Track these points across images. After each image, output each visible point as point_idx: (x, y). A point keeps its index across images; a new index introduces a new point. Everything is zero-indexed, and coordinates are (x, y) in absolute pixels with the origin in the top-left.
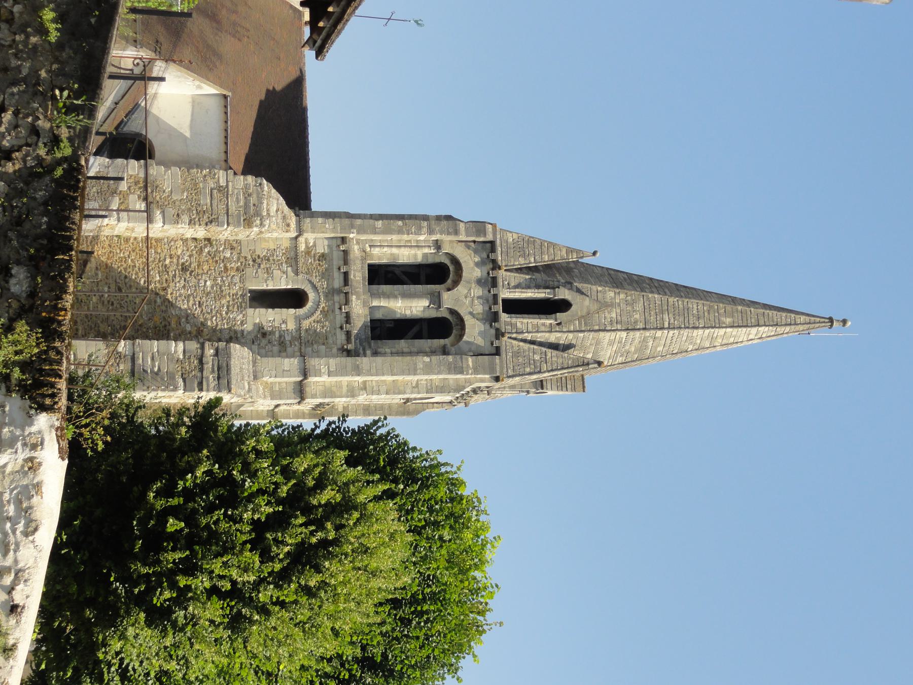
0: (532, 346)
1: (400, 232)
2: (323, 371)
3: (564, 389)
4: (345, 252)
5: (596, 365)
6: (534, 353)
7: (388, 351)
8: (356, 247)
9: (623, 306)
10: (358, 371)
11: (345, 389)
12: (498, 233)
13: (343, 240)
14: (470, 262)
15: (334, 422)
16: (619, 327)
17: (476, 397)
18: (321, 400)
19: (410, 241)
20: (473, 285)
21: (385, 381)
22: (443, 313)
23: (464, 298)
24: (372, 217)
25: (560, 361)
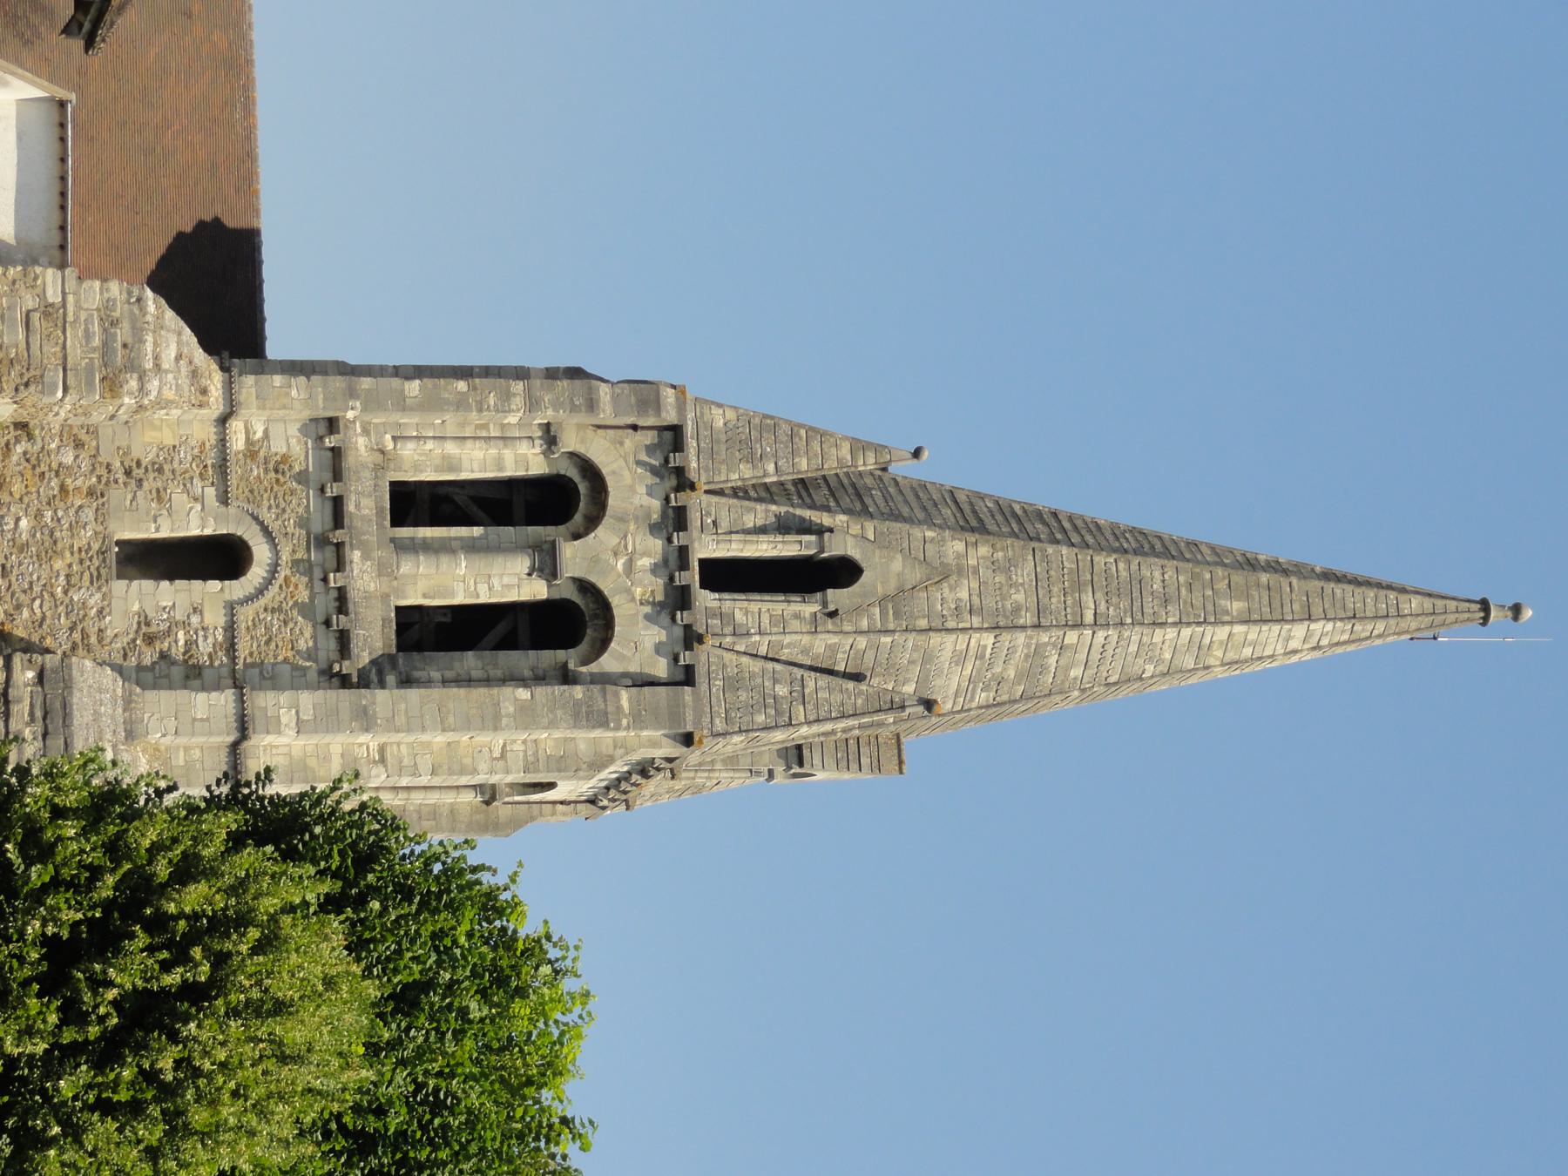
0: (770, 665)
1: (461, 404)
2: (284, 720)
3: (854, 766)
4: (336, 452)
5: (921, 708)
6: (775, 681)
7: (436, 675)
8: (361, 442)
10: (365, 719)
12: (690, 407)
13: (332, 424)
14: (632, 489)
16: (976, 621)
19: (485, 427)
20: (632, 527)
23: (617, 558)
24: (399, 372)
25: (837, 698)
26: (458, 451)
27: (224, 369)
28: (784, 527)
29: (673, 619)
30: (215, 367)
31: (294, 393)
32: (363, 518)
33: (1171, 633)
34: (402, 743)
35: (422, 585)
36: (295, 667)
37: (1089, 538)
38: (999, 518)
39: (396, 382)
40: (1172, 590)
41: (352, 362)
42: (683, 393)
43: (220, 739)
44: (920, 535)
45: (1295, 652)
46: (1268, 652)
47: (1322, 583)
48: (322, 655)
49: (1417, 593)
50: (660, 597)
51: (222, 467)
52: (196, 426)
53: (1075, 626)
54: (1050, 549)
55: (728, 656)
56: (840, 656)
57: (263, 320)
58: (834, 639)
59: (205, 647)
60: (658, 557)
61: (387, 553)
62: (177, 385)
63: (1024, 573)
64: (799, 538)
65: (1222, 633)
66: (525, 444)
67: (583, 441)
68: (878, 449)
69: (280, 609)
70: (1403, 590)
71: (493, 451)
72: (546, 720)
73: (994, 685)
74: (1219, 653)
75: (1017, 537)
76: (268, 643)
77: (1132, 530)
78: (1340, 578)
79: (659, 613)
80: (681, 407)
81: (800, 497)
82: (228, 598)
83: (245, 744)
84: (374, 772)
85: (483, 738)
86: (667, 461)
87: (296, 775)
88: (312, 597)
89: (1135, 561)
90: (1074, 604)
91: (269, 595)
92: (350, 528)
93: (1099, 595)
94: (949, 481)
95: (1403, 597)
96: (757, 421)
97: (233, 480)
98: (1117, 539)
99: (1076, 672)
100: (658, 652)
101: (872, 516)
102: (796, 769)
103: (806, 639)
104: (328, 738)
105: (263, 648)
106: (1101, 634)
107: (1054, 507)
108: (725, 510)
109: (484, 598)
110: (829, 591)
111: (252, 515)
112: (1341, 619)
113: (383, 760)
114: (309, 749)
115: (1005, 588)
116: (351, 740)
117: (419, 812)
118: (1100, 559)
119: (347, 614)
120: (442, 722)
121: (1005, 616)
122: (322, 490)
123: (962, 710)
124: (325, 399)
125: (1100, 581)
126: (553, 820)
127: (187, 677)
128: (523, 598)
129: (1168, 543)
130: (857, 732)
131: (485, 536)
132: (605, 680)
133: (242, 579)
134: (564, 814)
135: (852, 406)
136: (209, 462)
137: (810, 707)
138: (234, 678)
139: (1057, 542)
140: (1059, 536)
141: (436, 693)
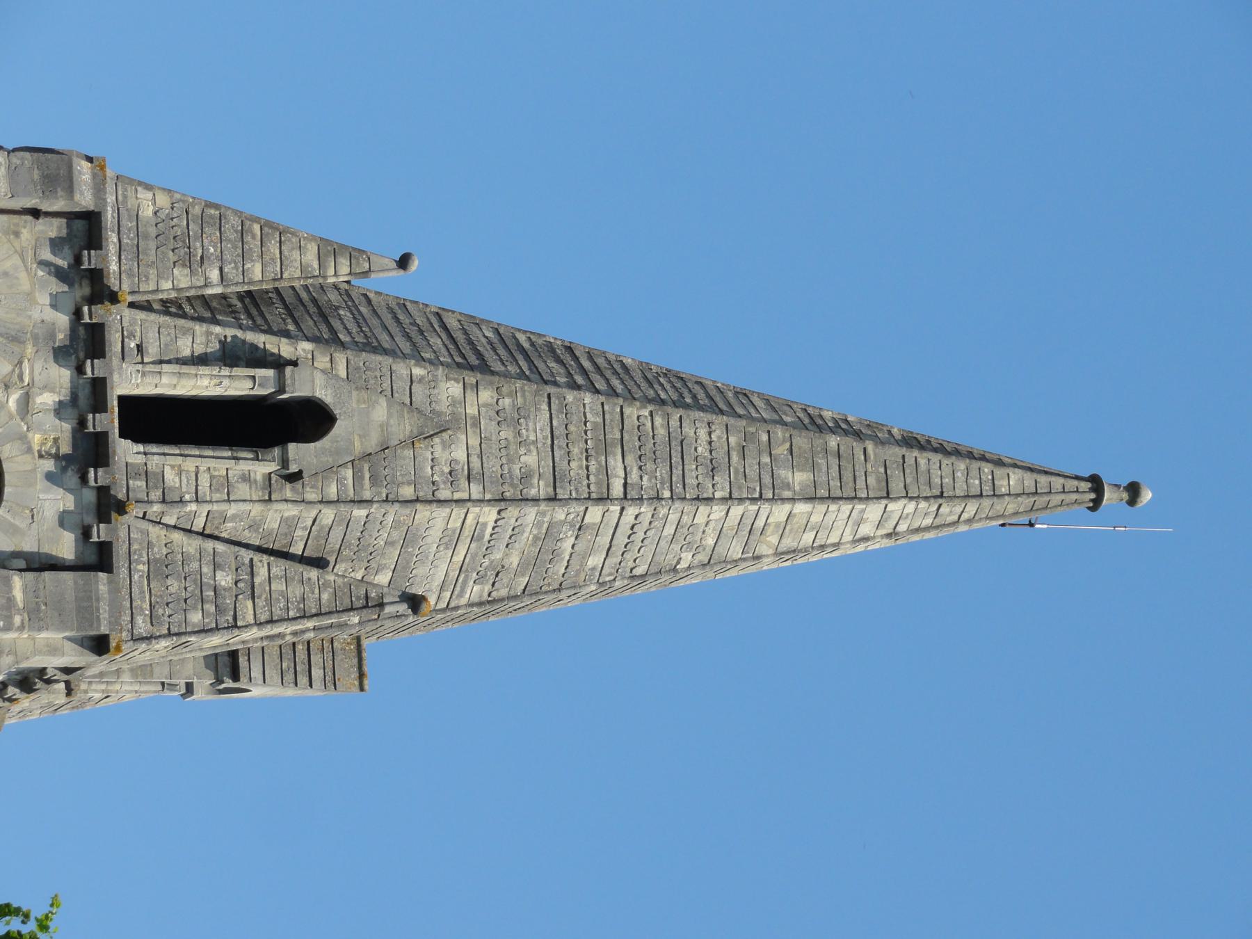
0: (209, 545)
3: (303, 680)
5: (403, 608)
6: (216, 567)
12: (110, 187)
20: (30, 350)
25: (296, 591)
28: (231, 356)
29: (84, 479)
33: (718, 511)
37: (615, 382)
38: (502, 351)
40: (720, 454)
42: (102, 168)
44: (405, 372)
45: (865, 539)
46: (833, 539)
47: (903, 451)
49: (1015, 466)
50: (66, 449)
53: (600, 500)
54: (570, 396)
55: (155, 531)
56: (299, 533)
58: (291, 511)
60: (64, 394)
63: (537, 427)
64: (251, 372)
65: (780, 512)
68: (354, 254)
70: (999, 463)
73: (491, 576)
74: (774, 539)
75: (528, 379)
77: (667, 374)
78: (923, 445)
79: (64, 469)
80: (99, 187)
81: (250, 316)
86: (78, 260)
89: (676, 414)
90: (598, 471)
93: (630, 459)
95: (999, 472)
96: (197, 210)
98: (651, 385)
99: (595, 561)
100: (62, 524)
101: (343, 345)
102: (229, 684)
103: (257, 509)
106: (631, 511)
107: (568, 338)
108: (151, 330)
110: (292, 447)
112: (926, 498)
115: (513, 447)
118: (631, 412)
121: (512, 485)
125: (631, 441)
129: (713, 393)
130: (311, 635)
135: (320, 201)
137: (261, 603)
139: (579, 388)
140: (580, 380)
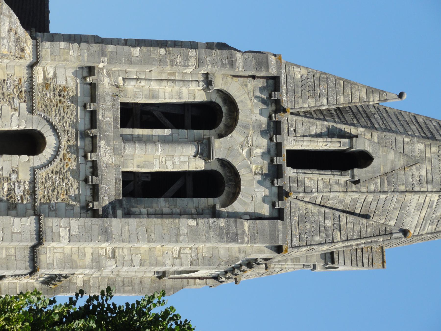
0: (323, 209)
1: (162, 61)
2: (62, 234)
3: (360, 264)
4: (93, 86)
5: (400, 235)
6: (325, 218)
7: (144, 211)
8: (106, 80)
9: (435, 161)
10: (106, 235)
11: (88, 258)
12: (283, 66)
13: (91, 70)
14: (251, 111)
15: (96, 298)
16: (430, 188)
17: (249, 272)
18: (57, 272)
19: (173, 74)
20: (251, 132)
21: (139, 249)
22: (215, 166)
23: (243, 148)
24: (126, 42)
25: (357, 228)
26: (158, 87)
27: (34, 38)
28: (331, 134)
29: (273, 183)
30: (28, 36)
31: (71, 52)
32: (107, 123)
34: (124, 249)
35: (137, 160)
36: (68, 205)
39: (127, 48)
41: (102, 36)
42: (280, 59)
43: (26, 244)
44: (401, 140)
48: (83, 199)
50: (265, 171)
51: (31, 92)
52: (17, 69)
55: (301, 204)
56: (358, 204)
57: (48, 12)
58: (356, 196)
59: (19, 192)
60: (265, 149)
61: (118, 142)
62: (9, 46)
66: (195, 84)
67: (225, 83)
69: (60, 172)
71: (177, 88)
72: (204, 238)
73: (436, 221)
76: (53, 190)
79: (265, 179)
80: (279, 67)
81: (339, 117)
82: (32, 165)
83: (40, 247)
84: (109, 263)
85: (169, 246)
86: (270, 96)
87: (67, 265)
88: (78, 167)
91: (54, 164)
92: (99, 128)
94: (414, 111)
96: (318, 75)
97: (36, 99)
100: (264, 201)
102: (330, 265)
103: (342, 195)
104: (85, 245)
105: (51, 193)
109: (170, 169)
110: (356, 170)
111: (46, 119)
113: (114, 257)
114: (74, 250)
116: (97, 246)
117: (123, 282)
119: (97, 176)
120: (148, 237)
122: (85, 106)
123: (418, 235)
124: (88, 56)
126: (193, 287)
127: (9, 209)
128: (191, 169)
130: (363, 246)
131: (172, 135)
132: (236, 216)
133: (40, 155)
134: (200, 284)
135: (368, 70)
136: (23, 89)
137: (343, 233)
138: (35, 210)
141: (145, 221)
